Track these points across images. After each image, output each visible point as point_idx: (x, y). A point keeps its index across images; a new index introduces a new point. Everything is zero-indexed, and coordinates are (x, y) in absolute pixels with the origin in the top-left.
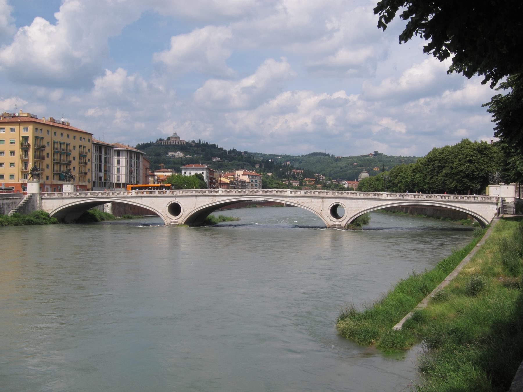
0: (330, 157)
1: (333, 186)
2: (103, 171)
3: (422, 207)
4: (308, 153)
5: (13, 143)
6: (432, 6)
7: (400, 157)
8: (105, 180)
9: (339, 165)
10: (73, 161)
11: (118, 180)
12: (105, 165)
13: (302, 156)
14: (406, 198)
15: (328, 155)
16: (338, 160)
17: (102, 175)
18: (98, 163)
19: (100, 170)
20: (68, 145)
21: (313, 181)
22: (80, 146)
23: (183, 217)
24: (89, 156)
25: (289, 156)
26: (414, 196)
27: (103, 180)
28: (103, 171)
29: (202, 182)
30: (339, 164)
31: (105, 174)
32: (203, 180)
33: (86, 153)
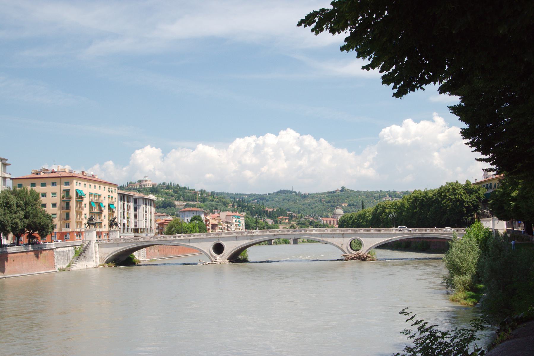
0: (297, 195)
1: (308, 223)
2: (126, 218)
3: (439, 240)
4: (275, 191)
5: (53, 194)
6: (501, 127)
7: (367, 192)
8: (128, 226)
9: (306, 201)
10: (85, 209)
11: (136, 226)
12: (128, 213)
13: (269, 194)
14: (265, 233)
15: (295, 192)
16: (305, 197)
17: (125, 221)
18: (122, 211)
19: (124, 218)
20: (100, 196)
21: (287, 219)
22: (91, 194)
23: (226, 255)
24: (115, 205)
25: (254, 195)
26: (270, 232)
27: (126, 226)
28: (126, 218)
29: (201, 223)
30: (307, 201)
31: (128, 221)
32: (202, 222)
33: (113, 202)
